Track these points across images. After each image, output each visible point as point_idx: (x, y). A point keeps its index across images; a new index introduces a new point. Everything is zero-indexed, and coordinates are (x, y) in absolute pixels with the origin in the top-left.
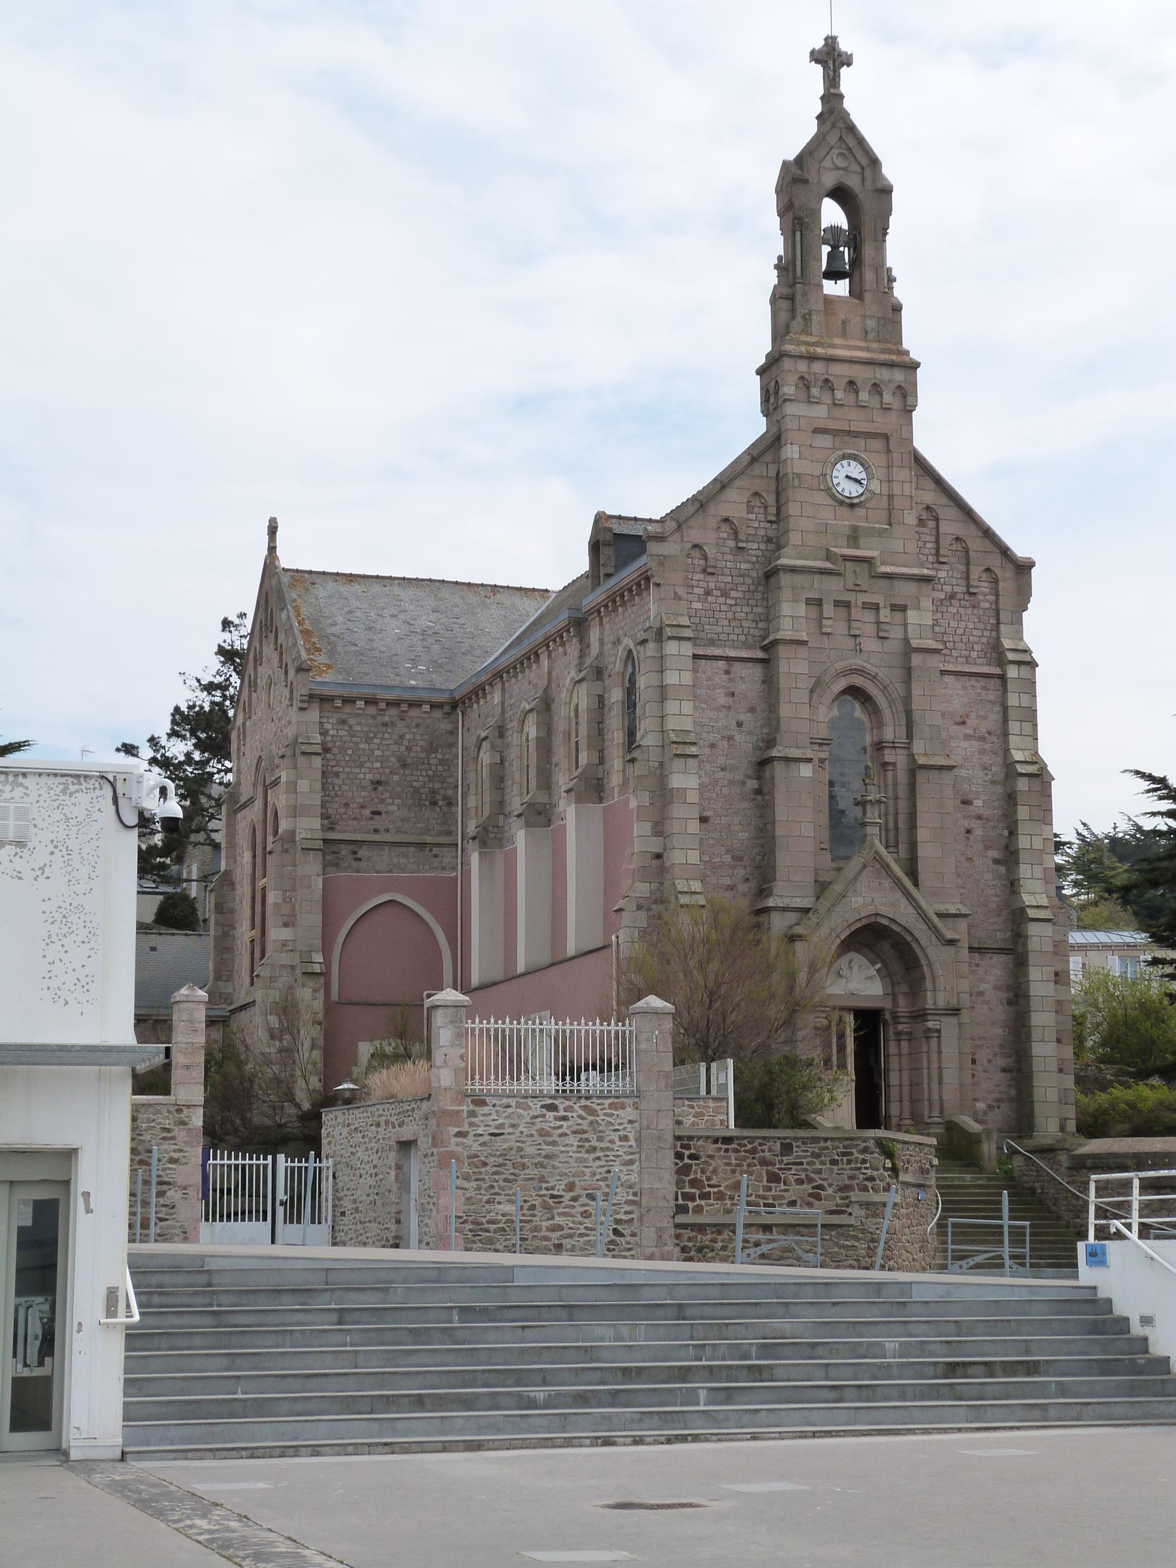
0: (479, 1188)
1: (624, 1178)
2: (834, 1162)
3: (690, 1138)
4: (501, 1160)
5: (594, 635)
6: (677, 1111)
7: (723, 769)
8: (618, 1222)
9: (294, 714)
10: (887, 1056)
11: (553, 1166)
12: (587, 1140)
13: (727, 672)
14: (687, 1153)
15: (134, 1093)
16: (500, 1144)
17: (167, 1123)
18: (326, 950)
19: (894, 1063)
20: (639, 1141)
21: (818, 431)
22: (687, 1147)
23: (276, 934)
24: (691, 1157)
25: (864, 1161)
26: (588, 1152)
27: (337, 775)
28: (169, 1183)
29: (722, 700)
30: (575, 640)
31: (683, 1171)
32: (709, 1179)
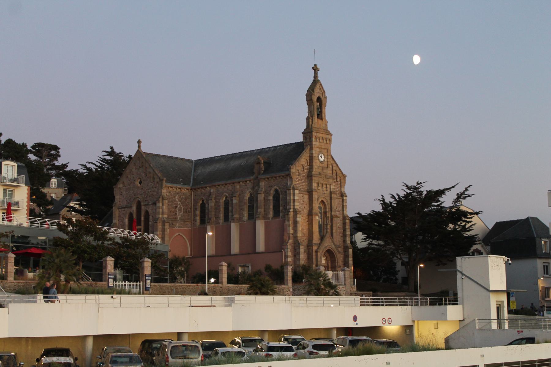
21: (318, 148)
29: (302, 202)
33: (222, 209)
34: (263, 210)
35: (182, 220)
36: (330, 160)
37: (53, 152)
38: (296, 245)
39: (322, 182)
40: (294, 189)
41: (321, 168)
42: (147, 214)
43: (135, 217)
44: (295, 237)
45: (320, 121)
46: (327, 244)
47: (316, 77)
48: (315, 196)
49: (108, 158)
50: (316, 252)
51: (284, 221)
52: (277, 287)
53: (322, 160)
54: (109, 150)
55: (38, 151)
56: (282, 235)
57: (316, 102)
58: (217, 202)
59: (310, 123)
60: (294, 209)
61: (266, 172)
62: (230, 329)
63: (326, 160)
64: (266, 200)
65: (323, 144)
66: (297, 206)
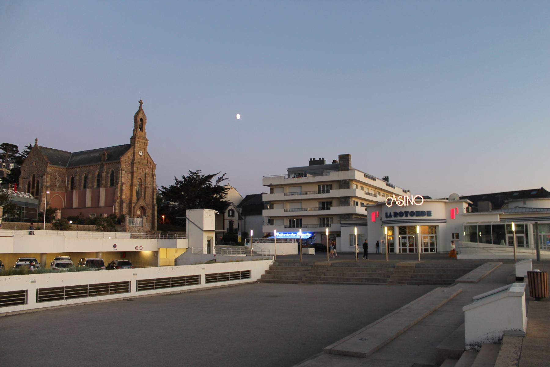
33: (83, 181)
34: (104, 182)
35: (60, 187)
36: (146, 155)
37: (14, 149)
38: (122, 203)
40: (122, 170)
42: (38, 182)
43: (31, 183)
44: (121, 198)
45: (141, 132)
46: (141, 203)
47: (140, 107)
48: (135, 175)
49: (29, 150)
50: (134, 207)
51: (115, 189)
52: (117, 227)
53: (141, 154)
54: (29, 146)
55: (5, 148)
56: (114, 197)
57: (140, 121)
58: (80, 177)
60: (122, 182)
61: (108, 160)
62: (12, 252)
64: (106, 176)
66: (123, 180)
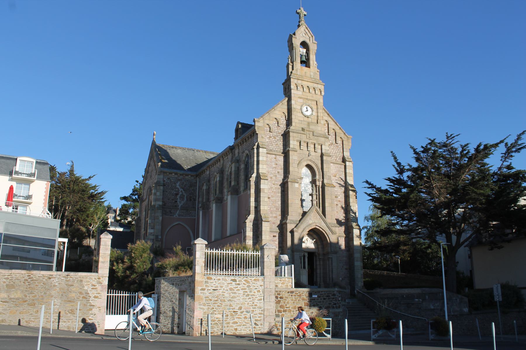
0: (209, 308)
1: (258, 305)
2: (324, 299)
3: (280, 292)
4: (216, 299)
5: (237, 152)
6: (276, 282)
7: (274, 184)
8: (256, 320)
9: (156, 176)
10: (316, 265)
11: (235, 301)
12: (246, 292)
13: (275, 158)
14: (279, 296)
15: (62, 271)
16: (216, 293)
17: (94, 283)
18: (162, 235)
19: (318, 267)
20: (264, 292)
21: (300, 98)
22: (279, 294)
23: (150, 231)
24: (281, 298)
25: (333, 298)
26: (246, 296)
27: (167, 192)
28: (94, 306)
29: (274, 166)
30: (231, 154)
31: (278, 302)
32: (286, 305)
39: (308, 140)
41: (306, 123)
48: (293, 157)
53: (309, 113)
59: (290, 70)
63: (315, 113)
65: (309, 94)
